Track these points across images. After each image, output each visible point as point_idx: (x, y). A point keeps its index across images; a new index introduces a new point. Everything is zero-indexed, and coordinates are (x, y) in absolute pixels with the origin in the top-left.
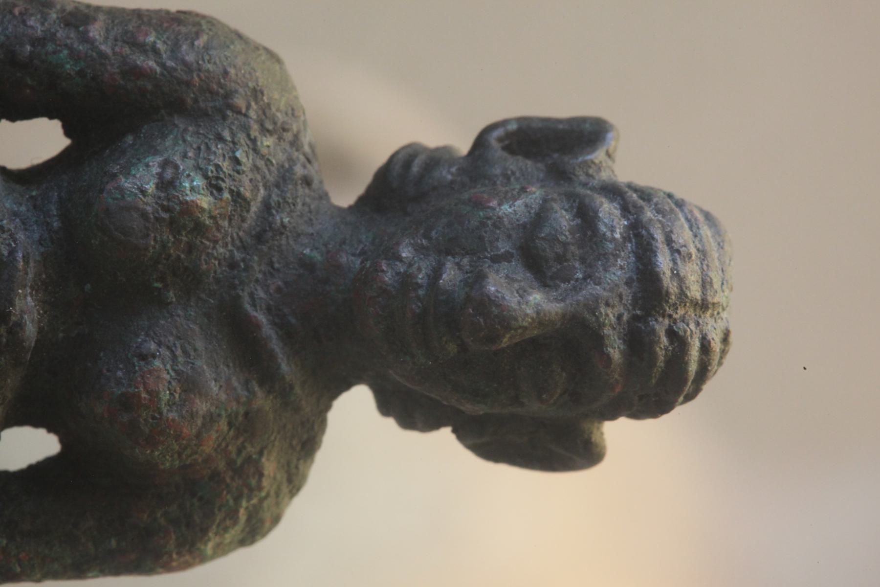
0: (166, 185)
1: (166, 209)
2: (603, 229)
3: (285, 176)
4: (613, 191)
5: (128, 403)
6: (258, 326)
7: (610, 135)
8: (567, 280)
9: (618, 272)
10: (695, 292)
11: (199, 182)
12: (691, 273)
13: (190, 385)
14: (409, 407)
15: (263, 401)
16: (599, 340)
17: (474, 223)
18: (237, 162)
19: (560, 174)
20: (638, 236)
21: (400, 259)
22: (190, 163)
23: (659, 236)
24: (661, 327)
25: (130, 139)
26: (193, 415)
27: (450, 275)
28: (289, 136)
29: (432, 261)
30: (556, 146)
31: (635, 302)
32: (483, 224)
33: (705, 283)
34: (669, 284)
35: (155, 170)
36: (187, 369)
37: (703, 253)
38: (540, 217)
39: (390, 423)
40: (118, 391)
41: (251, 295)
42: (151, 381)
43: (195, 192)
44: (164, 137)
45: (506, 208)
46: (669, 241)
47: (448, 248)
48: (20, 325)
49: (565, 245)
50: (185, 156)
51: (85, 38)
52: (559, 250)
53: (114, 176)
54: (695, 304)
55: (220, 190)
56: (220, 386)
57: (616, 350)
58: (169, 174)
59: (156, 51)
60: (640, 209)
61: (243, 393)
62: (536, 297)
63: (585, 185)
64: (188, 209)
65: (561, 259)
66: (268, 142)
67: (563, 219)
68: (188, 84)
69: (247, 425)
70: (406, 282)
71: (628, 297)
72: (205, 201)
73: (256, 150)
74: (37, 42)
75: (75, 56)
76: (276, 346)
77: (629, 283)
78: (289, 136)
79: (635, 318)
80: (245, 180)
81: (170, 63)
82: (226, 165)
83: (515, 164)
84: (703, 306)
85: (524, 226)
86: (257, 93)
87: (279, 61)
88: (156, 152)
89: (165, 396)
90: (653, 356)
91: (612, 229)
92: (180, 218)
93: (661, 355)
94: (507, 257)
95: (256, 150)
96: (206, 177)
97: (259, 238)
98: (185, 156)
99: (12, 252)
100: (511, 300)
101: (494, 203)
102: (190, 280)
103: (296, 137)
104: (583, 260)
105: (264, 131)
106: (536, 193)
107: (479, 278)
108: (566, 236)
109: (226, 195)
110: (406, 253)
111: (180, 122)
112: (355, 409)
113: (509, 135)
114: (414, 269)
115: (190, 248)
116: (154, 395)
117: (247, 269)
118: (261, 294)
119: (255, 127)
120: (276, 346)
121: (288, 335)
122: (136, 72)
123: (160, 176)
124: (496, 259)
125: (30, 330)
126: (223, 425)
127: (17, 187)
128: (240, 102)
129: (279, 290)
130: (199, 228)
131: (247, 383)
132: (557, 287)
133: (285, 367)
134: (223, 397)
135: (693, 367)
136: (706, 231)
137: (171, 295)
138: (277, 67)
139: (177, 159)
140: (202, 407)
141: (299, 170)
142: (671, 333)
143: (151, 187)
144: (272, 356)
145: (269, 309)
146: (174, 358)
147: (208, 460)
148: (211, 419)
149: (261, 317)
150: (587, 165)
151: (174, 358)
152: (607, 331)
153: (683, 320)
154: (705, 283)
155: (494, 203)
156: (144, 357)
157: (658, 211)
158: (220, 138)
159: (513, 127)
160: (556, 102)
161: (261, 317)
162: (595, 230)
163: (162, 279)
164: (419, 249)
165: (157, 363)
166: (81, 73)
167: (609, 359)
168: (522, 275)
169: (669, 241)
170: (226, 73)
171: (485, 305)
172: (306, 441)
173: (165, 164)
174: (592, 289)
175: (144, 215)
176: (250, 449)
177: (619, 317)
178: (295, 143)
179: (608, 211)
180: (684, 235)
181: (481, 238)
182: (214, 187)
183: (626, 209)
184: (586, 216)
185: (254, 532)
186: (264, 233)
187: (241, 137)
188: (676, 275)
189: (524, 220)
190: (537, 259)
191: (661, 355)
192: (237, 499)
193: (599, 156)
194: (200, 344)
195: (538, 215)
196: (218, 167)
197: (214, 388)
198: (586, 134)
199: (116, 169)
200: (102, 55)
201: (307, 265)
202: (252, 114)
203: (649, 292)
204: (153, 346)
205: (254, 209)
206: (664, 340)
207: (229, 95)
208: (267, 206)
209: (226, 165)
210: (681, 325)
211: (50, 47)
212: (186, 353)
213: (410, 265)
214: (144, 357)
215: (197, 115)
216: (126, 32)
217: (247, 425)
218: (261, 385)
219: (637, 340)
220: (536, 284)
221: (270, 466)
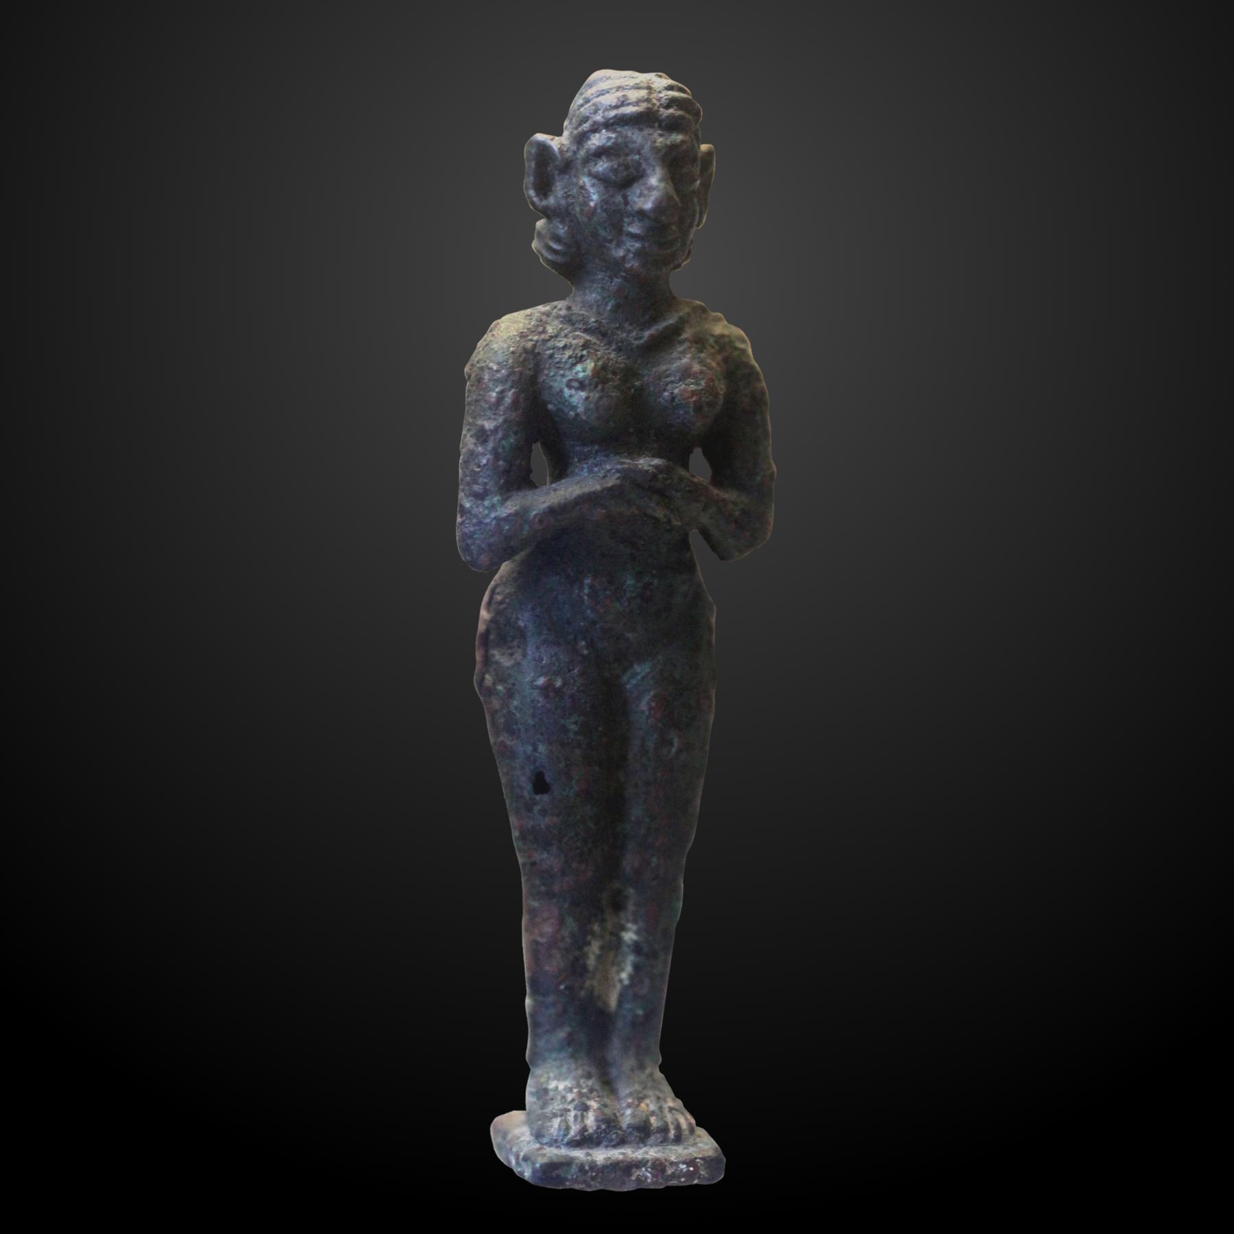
0: (582, 386)
1: (596, 386)
2: (609, 144)
5: (698, 408)
6: (652, 336)
8: (639, 164)
9: (636, 136)
10: (643, 93)
11: (579, 368)
13: (686, 373)
15: (687, 334)
16: (672, 147)
17: (604, 215)
18: (565, 347)
20: (612, 124)
21: (624, 258)
22: (567, 373)
23: (612, 113)
24: (666, 113)
25: (550, 407)
26: (701, 372)
27: (635, 229)
28: (544, 318)
29: (624, 238)
31: (652, 127)
32: (605, 211)
34: (644, 106)
35: (573, 392)
36: (678, 375)
38: (602, 179)
40: (692, 413)
41: (636, 339)
42: (687, 395)
43: (584, 370)
44: (551, 387)
45: (595, 197)
46: (616, 107)
47: (618, 229)
48: (656, 467)
49: (619, 165)
50: (563, 376)
51: (496, 430)
52: (622, 168)
53: (577, 415)
54: (650, 93)
55: (582, 356)
56: (682, 359)
57: (678, 138)
58: (576, 384)
59: (502, 392)
60: (595, 123)
61: (687, 345)
62: (653, 181)
63: (575, 153)
64: (596, 373)
65: (627, 167)
66: (550, 330)
67: (602, 166)
68: (521, 373)
70: (639, 254)
71: (650, 131)
72: (590, 365)
73: (556, 336)
74: (497, 456)
75: (505, 437)
76: (662, 326)
77: (641, 130)
78: (544, 318)
79: (660, 127)
80: (574, 342)
81: (509, 384)
82: (568, 353)
83: (559, 189)
85: (606, 187)
86: (522, 336)
88: (561, 391)
89: (693, 387)
91: (609, 138)
92: (600, 377)
93: (679, 113)
94: (625, 197)
95: (556, 336)
96: (575, 364)
97: (604, 335)
98: (563, 376)
99: (618, 471)
100: (655, 195)
101: (592, 204)
102: (629, 374)
104: (627, 155)
105: (544, 332)
106: (586, 180)
107: (641, 214)
108: (615, 164)
109: (585, 352)
110: (621, 253)
111: (541, 379)
114: (632, 249)
115: (614, 373)
116: (694, 393)
117: (622, 342)
118: (634, 334)
119: (543, 336)
120: (662, 326)
121: (654, 320)
122: (515, 402)
123: (577, 389)
124: (626, 203)
125: (656, 461)
126: (703, 355)
127: (570, 470)
128: (529, 345)
129: (631, 324)
130: (604, 368)
131: (681, 343)
132: (644, 170)
133: (671, 322)
134: (689, 356)
137: (637, 383)
139: (565, 380)
140: (696, 367)
142: (667, 107)
143: (583, 394)
144: (666, 328)
145: (642, 330)
146: (672, 382)
147: (718, 364)
148: (701, 362)
149: (647, 334)
150: (561, 150)
151: (672, 382)
152: (668, 142)
153: (659, 100)
155: (592, 204)
156: (673, 398)
157: (596, 112)
158: (551, 356)
161: (647, 334)
162: (610, 148)
163: (629, 388)
164: (618, 245)
165: (676, 391)
166: (516, 433)
167: (683, 142)
168: (637, 189)
169: (616, 107)
170: (513, 353)
171: (659, 208)
173: (569, 386)
174: (646, 150)
175: (600, 398)
176: (711, 341)
177: (661, 135)
181: (614, 211)
182: (581, 359)
183: (595, 129)
184: (601, 153)
186: (600, 332)
187: (550, 344)
188: (637, 103)
189: (602, 188)
190: (627, 179)
191: (679, 113)
192: (736, 349)
194: (663, 368)
195: (600, 179)
196: (570, 357)
197: (685, 361)
199: (572, 413)
200: (505, 421)
201: (617, 307)
202: (536, 338)
204: (666, 394)
205: (588, 337)
206: (671, 111)
207: (526, 351)
208: (585, 331)
209: (568, 353)
210: (663, 101)
211: (500, 450)
212: (667, 376)
213: (629, 250)
214: (673, 398)
215: (538, 369)
216: (490, 408)
218: (680, 335)
219: (672, 126)
220: (641, 181)
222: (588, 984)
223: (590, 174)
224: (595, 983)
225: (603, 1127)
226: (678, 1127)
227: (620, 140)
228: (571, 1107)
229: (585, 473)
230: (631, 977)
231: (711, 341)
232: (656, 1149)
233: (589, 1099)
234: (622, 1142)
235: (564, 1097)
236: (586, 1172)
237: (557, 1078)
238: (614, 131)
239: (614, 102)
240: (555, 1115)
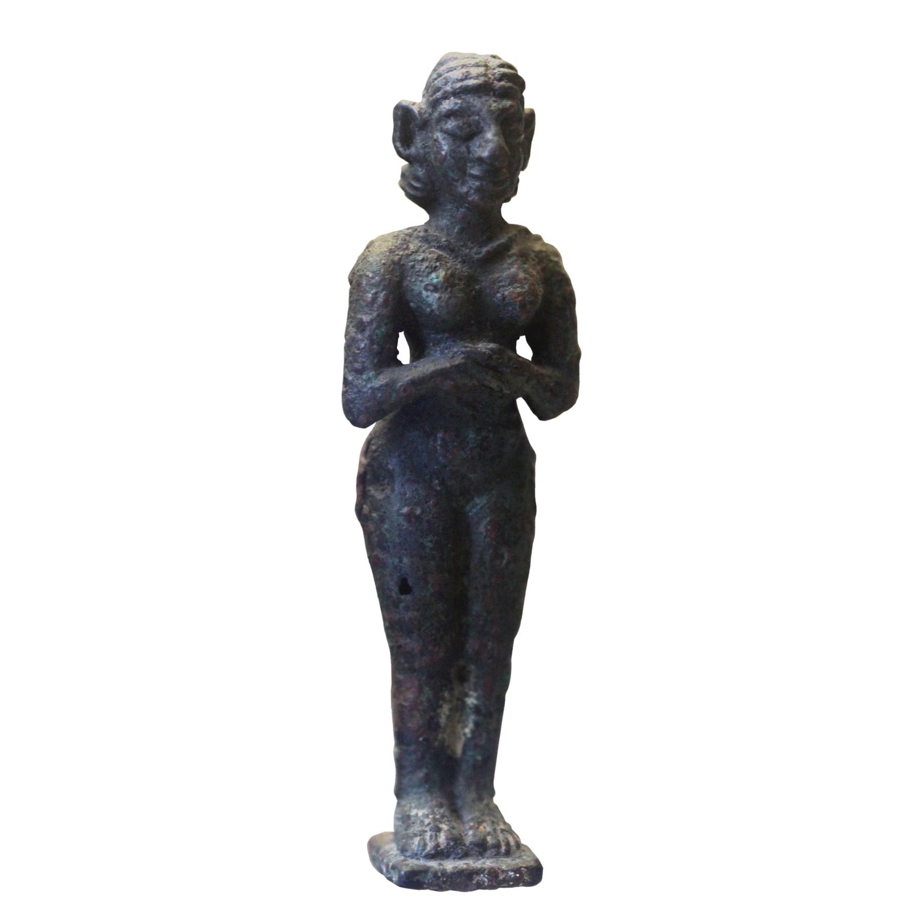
0: (436, 289)
1: (446, 289)
2: (456, 108)
3: (425, 240)
4: (435, 104)
5: (523, 306)
6: (488, 251)
7: (404, 104)
8: (479, 123)
9: (476, 102)
10: (481, 70)
11: (433, 275)
12: (474, 71)
13: (513, 280)
14: (509, 189)
15: (515, 250)
16: (504, 110)
17: (452, 161)
18: (423, 260)
19: (425, 125)
20: (459, 93)
21: (467, 193)
22: (425, 279)
23: (459, 85)
24: (498, 84)
25: (412, 304)
26: (525, 279)
27: (475, 171)
28: (407, 238)
29: (467, 178)
30: (407, 126)
31: (488, 95)
32: (453, 158)
33: (477, 65)
34: (482, 79)
35: (429, 293)
36: (508, 281)
37: (463, 66)
38: (450, 134)
39: (513, 199)
40: (518, 309)
41: (476, 254)
42: (514, 295)
43: (438, 277)
44: (412, 290)
45: (445, 148)
46: (462, 80)
47: (463, 172)
48: (491, 350)
49: (464, 124)
50: (422, 281)
51: (371, 322)
52: (466, 126)
53: (432, 311)
54: (487, 70)
55: (436, 267)
56: (511, 268)
58: (431, 288)
59: (376, 293)
60: (446, 92)
61: (514, 258)
62: (489, 135)
63: (430, 114)
64: (446, 279)
65: (469, 125)
66: (412, 247)
67: (451, 124)
68: (390, 280)
69: (524, 256)
70: (478, 190)
71: (487, 98)
72: (442, 273)
73: (417, 252)
74: (372, 341)
75: (378, 327)
76: (495, 244)
77: (480, 97)
78: (407, 238)
79: (494, 95)
80: (430, 256)
81: (381, 287)
82: (425, 264)
83: (418, 141)
84: (486, 66)
85: (454, 140)
86: (391, 251)
87: (371, 244)
88: (420, 293)
89: (519, 290)
90: (511, 88)
91: (456, 104)
92: (450, 282)
93: (509, 84)
94: (468, 148)
95: (417, 252)
96: (430, 273)
97: (452, 251)
98: (422, 281)
99: (463, 353)
100: (490, 146)
101: (443, 153)
102: (471, 280)
103: (407, 235)
104: (470, 116)
105: (407, 248)
106: (438, 135)
107: (480, 160)
108: (460, 123)
109: (438, 264)
110: (465, 189)
111: (405, 284)
112: (511, 212)
113: (403, 146)
114: (473, 187)
115: (460, 279)
116: (519, 294)
117: (466, 256)
118: (475, 250)
119: (406, 252)
120: (495, 244)
121: (490, 240)
122: (386, 301)
123: (432, 291)
124: (469, 152)
125: (491, 345)
126: (526, 266)
127: (426, 352)
128: (396, 258)
129: (472, 243)
130: (452, 275)
131: (510, 257)
132: (482, 128)
133: (502, 241)
134: (516, 266)
135: (511, 71)
136: (452, 64)
137: (477, 287)
138: (377, 244)
139: (423, 285)
140: (522, 275)
141: (421, 234)
142: (500, 80)
143: (437, 295)
144: (499, 246)
145: (481, 247)
146: (503, 286)
147: (538, 272)
148: (525, 271)
149: (484, 250)
150: (420, 113)
151: (503, 286)
152: (500, 107)
153: (493, 75)
154: (477, 65)
155: (443, 153)
156: (504, 298)
157: (446, 84)
158: (413, 267)
159: (398, 144)
160: (388, 126)
161: (484, 250)
162: (457, 111)
163: (471, 291)
164: (463, 184)
165: (506, 293)
166: (386, 324)
167: (511, 106)
168: (477, 141)
169: (462, 80)
170: (384, 264)
171: (493, 156)
172: (523, 232)
173: (426, 289)
174: (484, 112)
175: (450, 298)
176: (533, 255)
177: (495, 101)
178: (410, 235)
179: (446, 105)
180: (457, 74)
181: (460, 158)
182: (435, 269)
183: (446, 97)
184: (450, 114)
185: (557, 255)
186: (449, 248)
187: (412, 258)
188: (477, 77)
189: (451, 141)
190: (469, 134)
191: (509, 84)
192: (551, 261)
193: (416, 109)
194: (497, 275)
195: (449, 134)
196: (427, 267)
197: (513, 270)
198: (403, 115)
199: (428, 309)
200: (378, 315)
201: (462, 230)
202: (401, 253)
203: (484, 89)
204: (499, 295)
205: (440, 253)
206: (502, 83)
207: (394, 263)
208: (438, 248)
209: (425, 264)
210: (496, 76)
211: (375, 337)
212: (500, 282)
213: (471, 188)
214: (504, 298)
215: (402, 276)
216: (367, 306)
217: (524, 256)
218: (509, 251)
220: (480, 136)
221: (537, 247)
222: (440, 736)
223: (442, 131)
224: (445, 736)
225: (452, 844)
226: (508, 844)
227: (464, 105)
228: (427, 829)
229: (438, 354)
230: (473, 732)
231: (533, 255)
232: (491, 860)
233: (441, 823)
234: (465, 855)
235: (422, 822)
236: (439, 878)
237: (417, 807)
238: (460, 98)
239: (460, 76)
240: (415, 835)
